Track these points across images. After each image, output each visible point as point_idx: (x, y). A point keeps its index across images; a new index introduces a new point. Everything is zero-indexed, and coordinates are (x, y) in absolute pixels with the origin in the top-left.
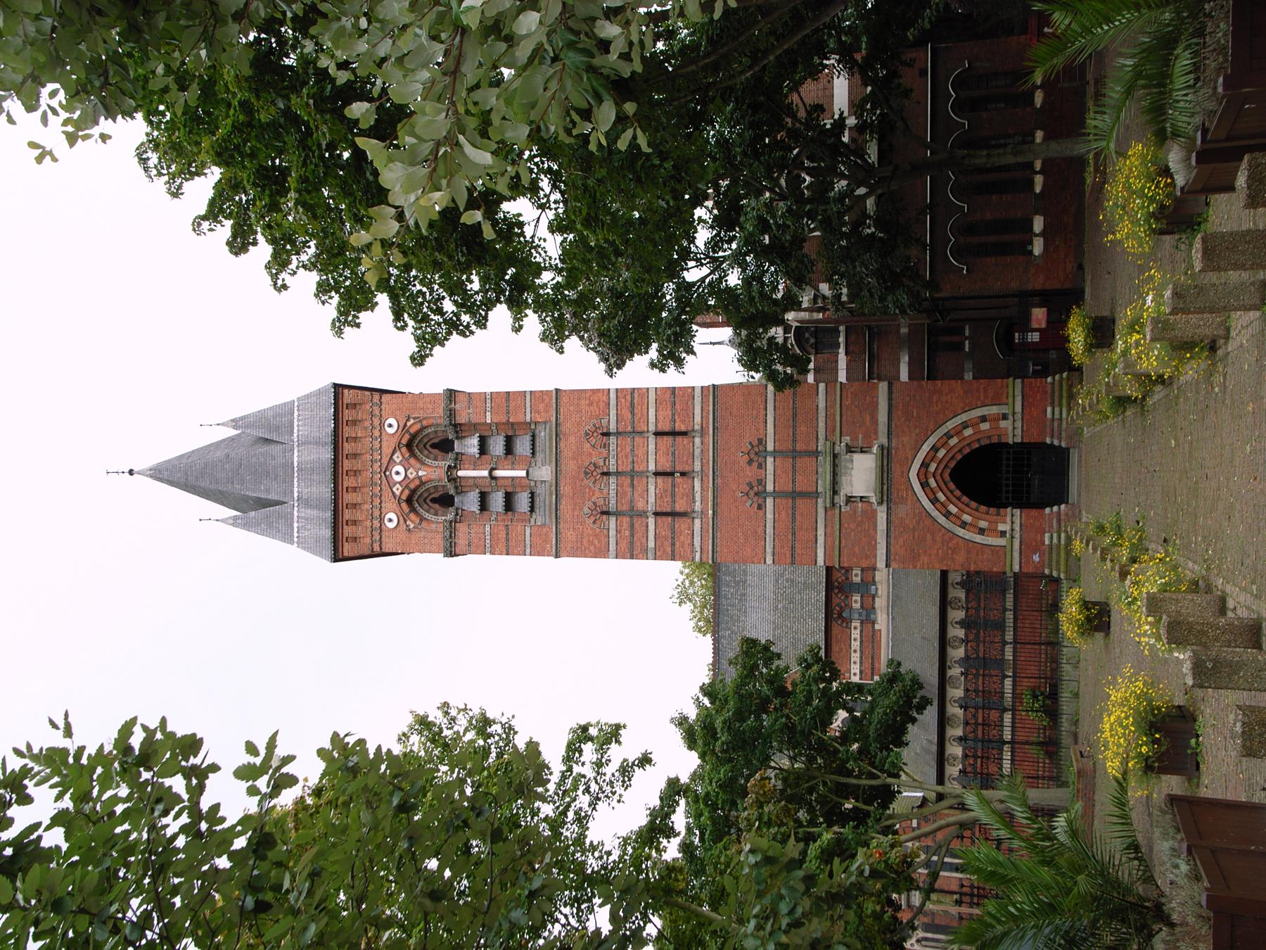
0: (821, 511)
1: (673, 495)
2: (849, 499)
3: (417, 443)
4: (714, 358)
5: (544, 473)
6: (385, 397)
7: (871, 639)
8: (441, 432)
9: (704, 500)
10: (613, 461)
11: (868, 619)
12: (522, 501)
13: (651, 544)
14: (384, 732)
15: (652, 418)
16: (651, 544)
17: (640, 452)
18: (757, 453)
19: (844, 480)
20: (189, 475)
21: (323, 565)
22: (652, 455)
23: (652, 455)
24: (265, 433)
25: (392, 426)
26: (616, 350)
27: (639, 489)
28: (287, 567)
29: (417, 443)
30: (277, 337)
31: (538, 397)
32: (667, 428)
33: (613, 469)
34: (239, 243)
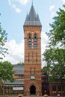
4: (44, 64)
5: (33, 48)
7: (17, 78)
8: (37, 38)
11: (19, 78)
12: (30, 46)
15: (38, 59)
18: (35, 68)
20: (32, 9)
21: (23, 24)
24: (37, 19)
26: (44, 55)
28: (23, 21)
30: (48, 18)
31: (40, 47)
34: (58, 13)
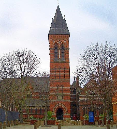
2: (57, 97)
5: (60, 61)
9: (57, 80)
12: (56, 58)
14: (20, 50)
20: (58, 12)
22: (62, 74)
23: (62, 74)
25: (65, 41)
27: (58, 72)
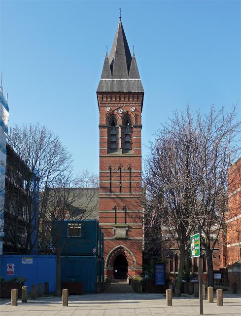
0: (112, 224)
1: (115, 187)
2: (115, 230)
3: (126, 117)
6: (140, 107)
10: (124, 171)
13: (103, 182)
16: (103, 182)
17: (126, 179)
19: (120, 229)
22: (125, 181)
29: (126, 117)
32: (132, 186)
33: (129, 181)
